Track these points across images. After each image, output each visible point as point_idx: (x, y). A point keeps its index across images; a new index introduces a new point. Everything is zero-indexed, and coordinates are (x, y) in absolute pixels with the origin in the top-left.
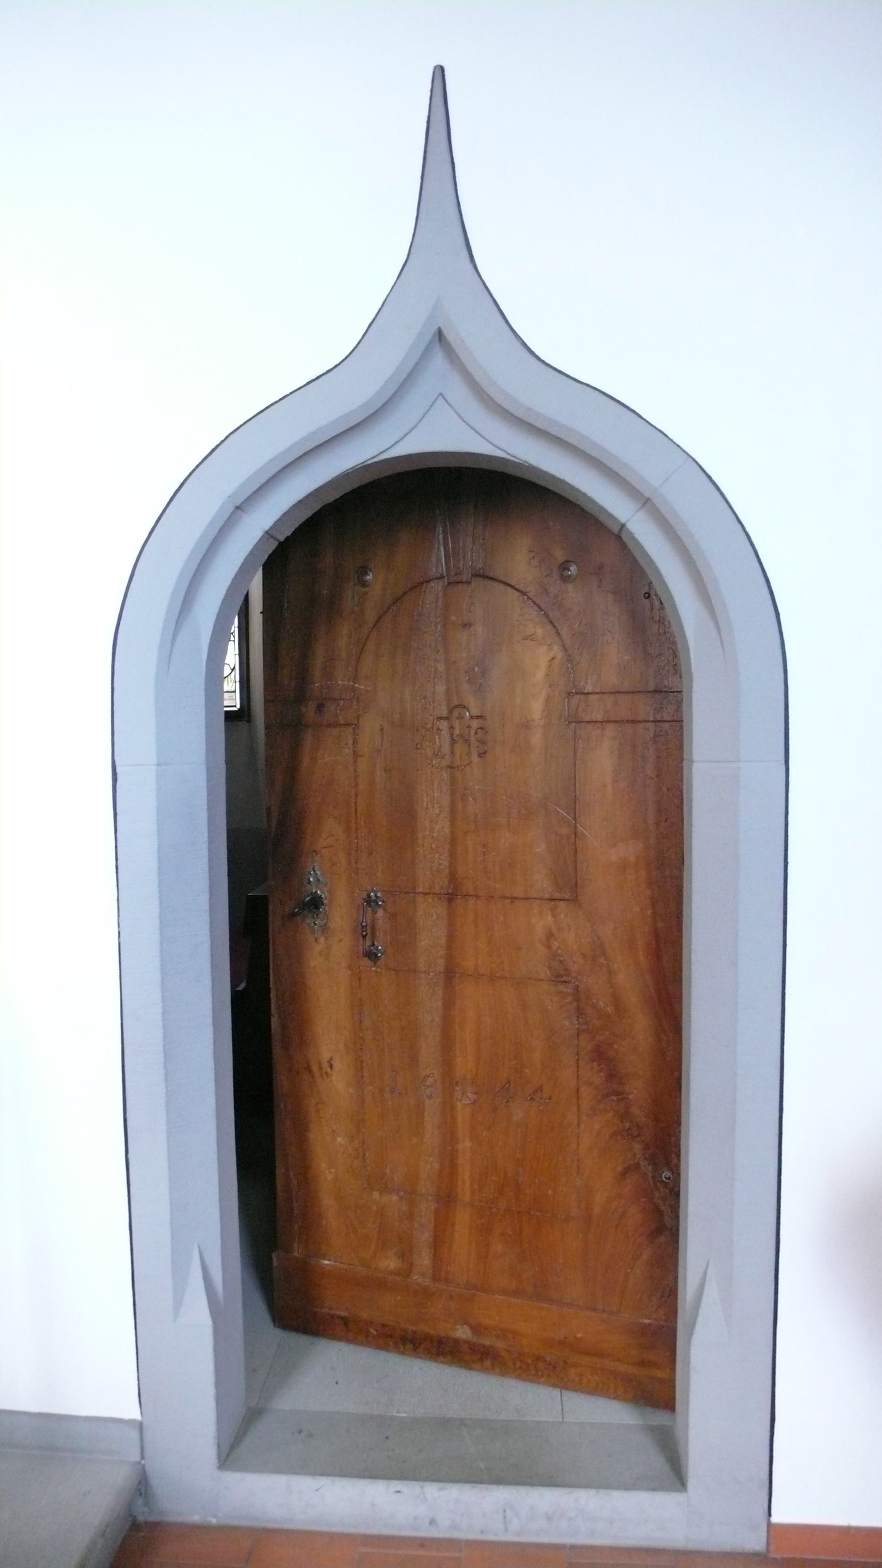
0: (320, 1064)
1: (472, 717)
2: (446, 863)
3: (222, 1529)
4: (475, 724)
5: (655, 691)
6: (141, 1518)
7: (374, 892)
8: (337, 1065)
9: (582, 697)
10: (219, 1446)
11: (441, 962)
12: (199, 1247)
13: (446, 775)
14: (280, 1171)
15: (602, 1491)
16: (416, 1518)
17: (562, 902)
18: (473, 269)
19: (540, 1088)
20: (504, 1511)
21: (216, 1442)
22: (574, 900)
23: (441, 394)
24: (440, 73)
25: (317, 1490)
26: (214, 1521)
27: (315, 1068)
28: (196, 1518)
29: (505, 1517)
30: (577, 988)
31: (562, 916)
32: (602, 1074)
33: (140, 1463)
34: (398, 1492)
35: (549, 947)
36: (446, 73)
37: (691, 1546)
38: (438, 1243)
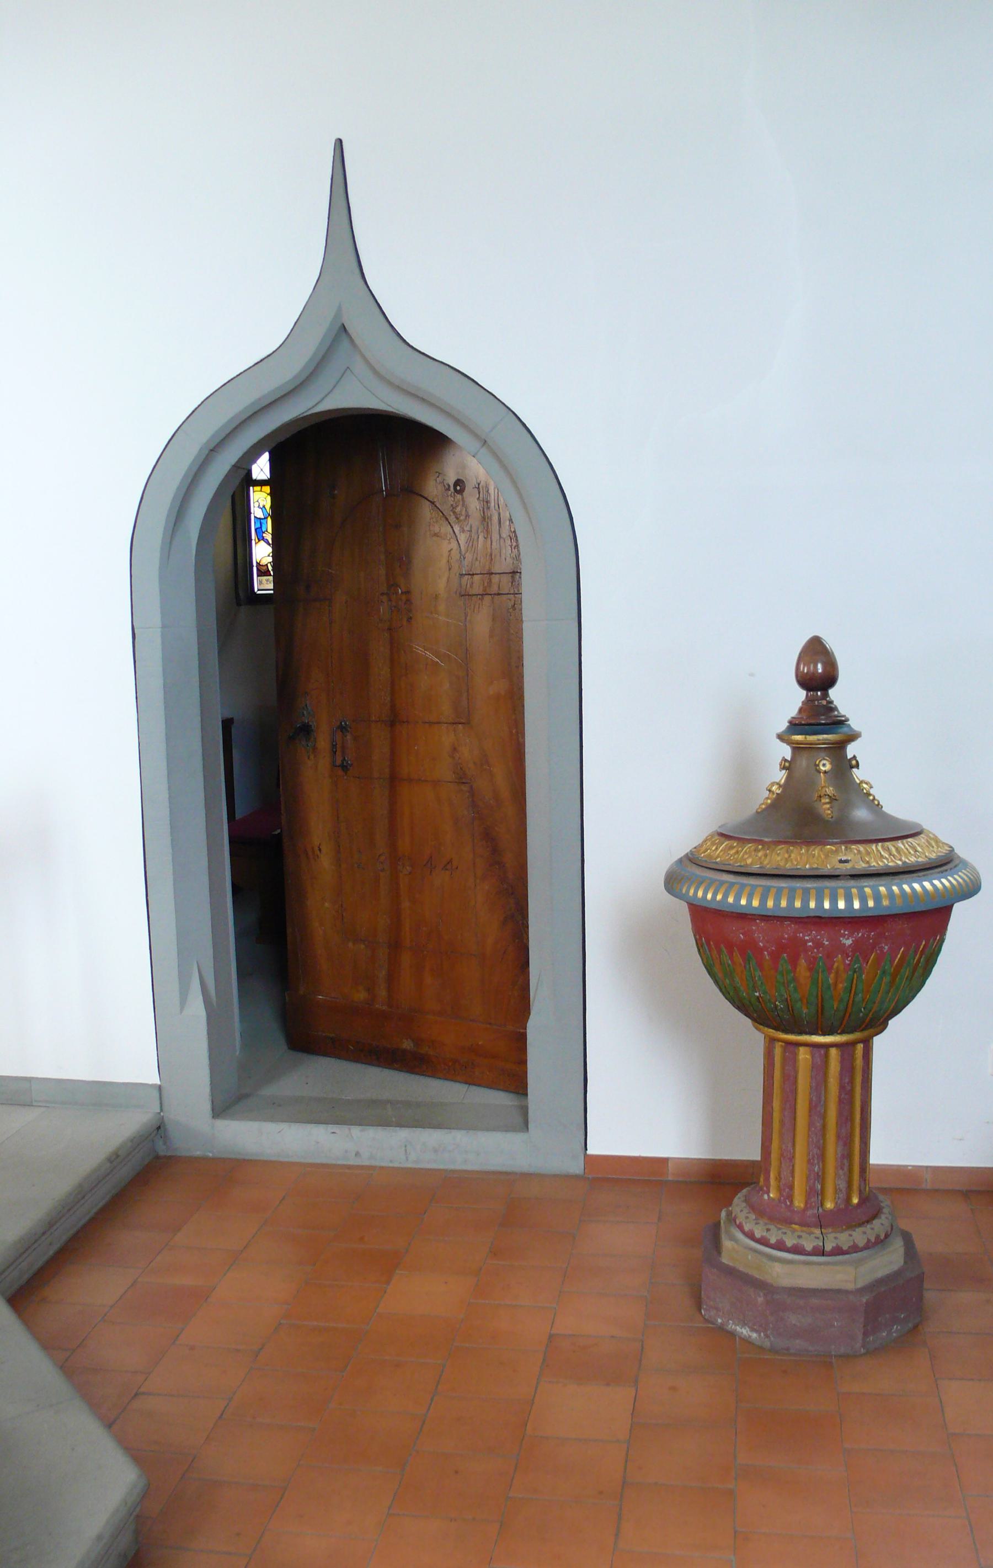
0: (313, 848)
1: (402, 593)
2: (389, 699)
3: (213, 1159)
4: (404, 597)
5: (473, 574)
6: (161, 1153)
7: (344, 721)
8: (324, 848)
9: (470, 576)
10: (213, 1102)
11: (387, 770)
12: (198, 966)
13: (386, 635)
14: (289, 930)
15: (471, 1132)
16: (346, 1151)
17: (460, 725)
18: (363, 283)
19: (450, 862)
20: (406, 1146)
21: (211, 1098)
22: (468, 723)
23: (348, 368)
24: (340, 142)
25: (280, 1132)
26: (211, 1155)
27: (310, 853)
28: (198, 1153)
29: (406, 1150)
30: (471, 787)
31: (461, 735)
32: (488, 849)
33: (159, 1113)
34: (333, 1133)
35: (453, 758)
36: (344, 144)
37: (532, 1170)
38: (391, 979)
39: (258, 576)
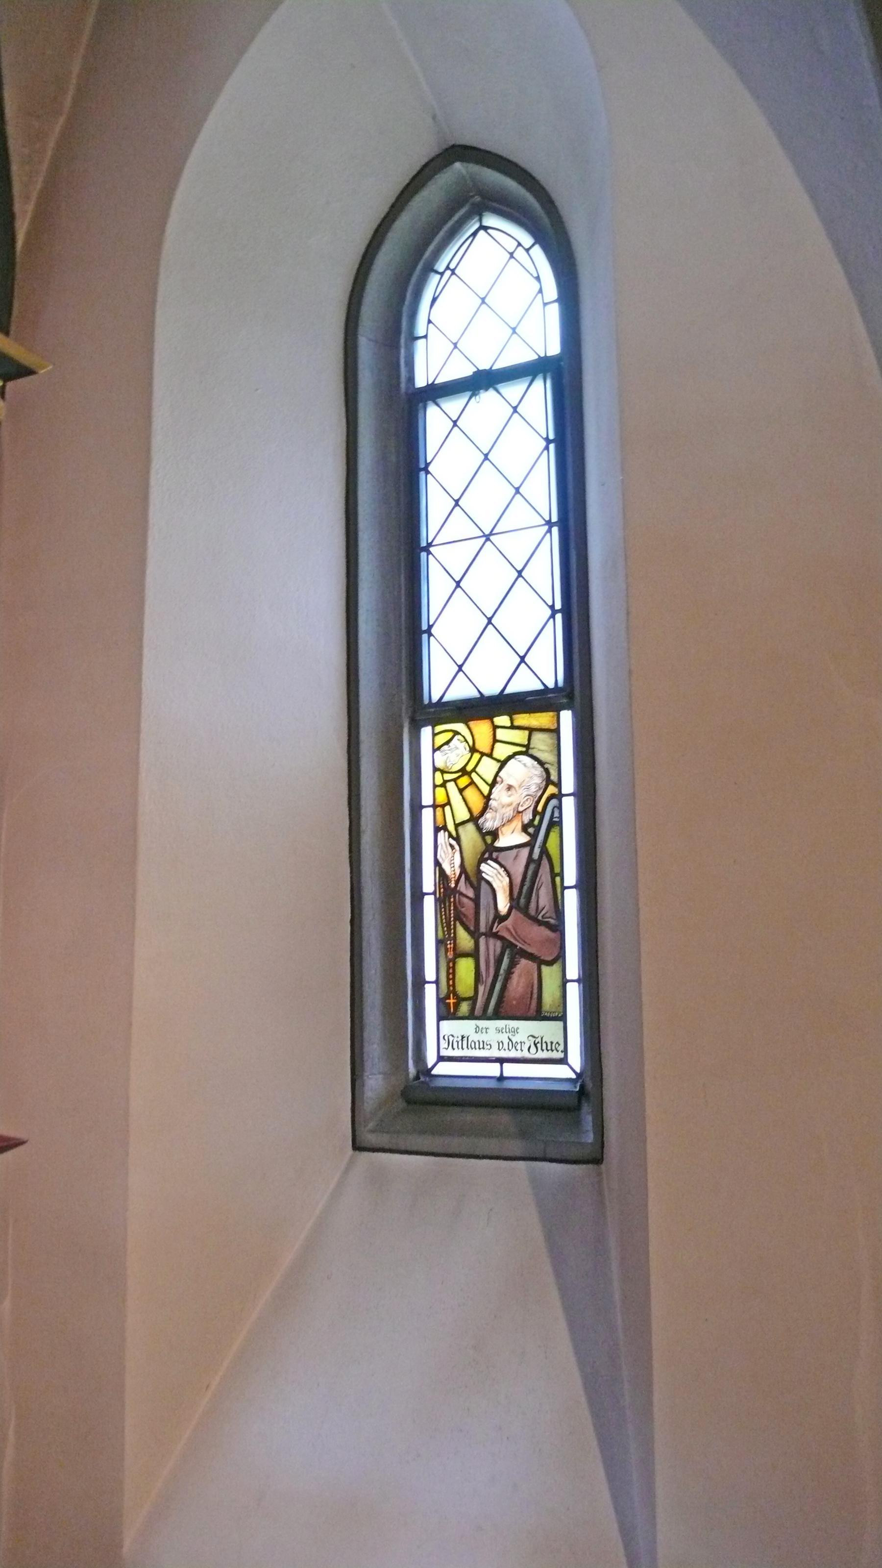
39: (440, 1018)
